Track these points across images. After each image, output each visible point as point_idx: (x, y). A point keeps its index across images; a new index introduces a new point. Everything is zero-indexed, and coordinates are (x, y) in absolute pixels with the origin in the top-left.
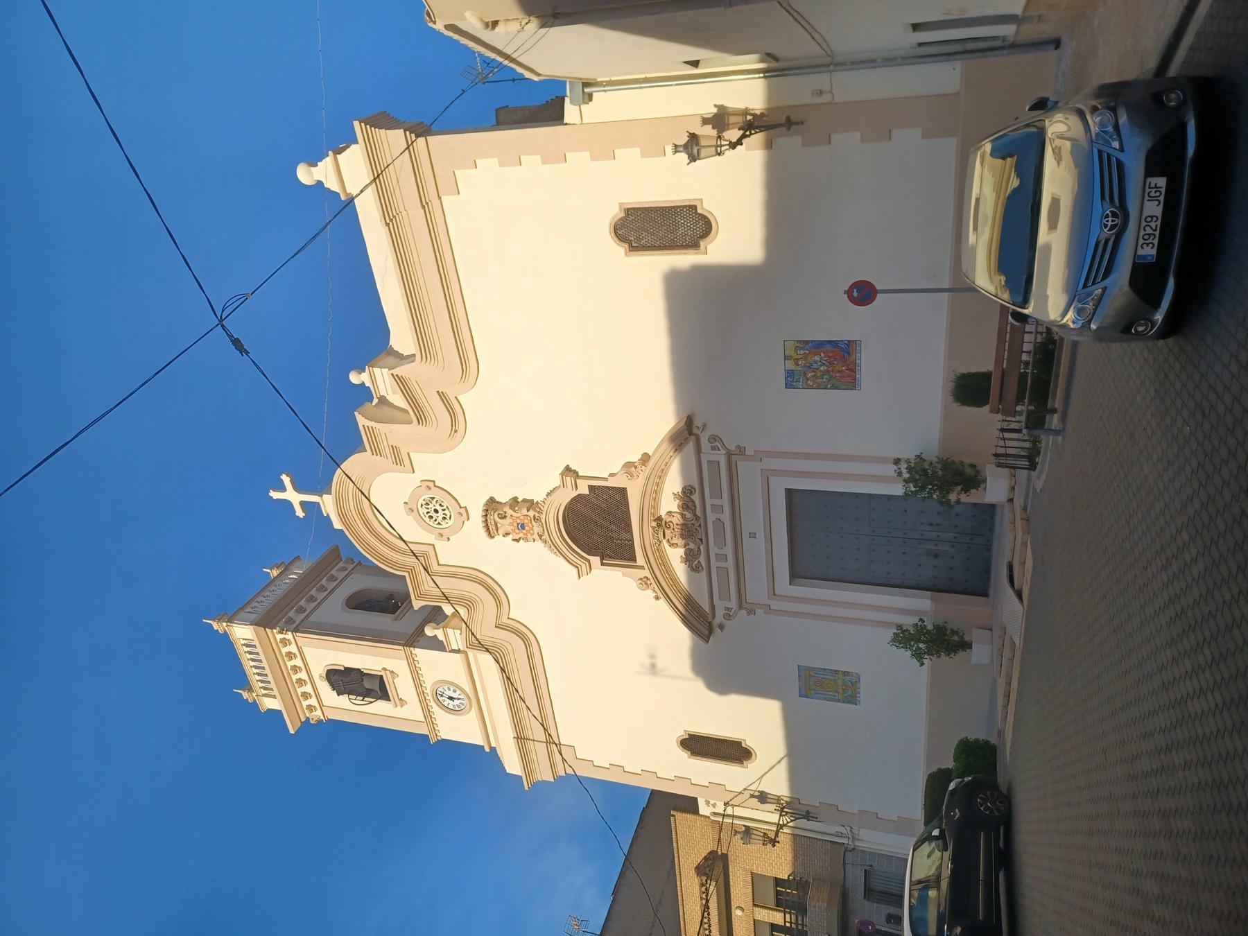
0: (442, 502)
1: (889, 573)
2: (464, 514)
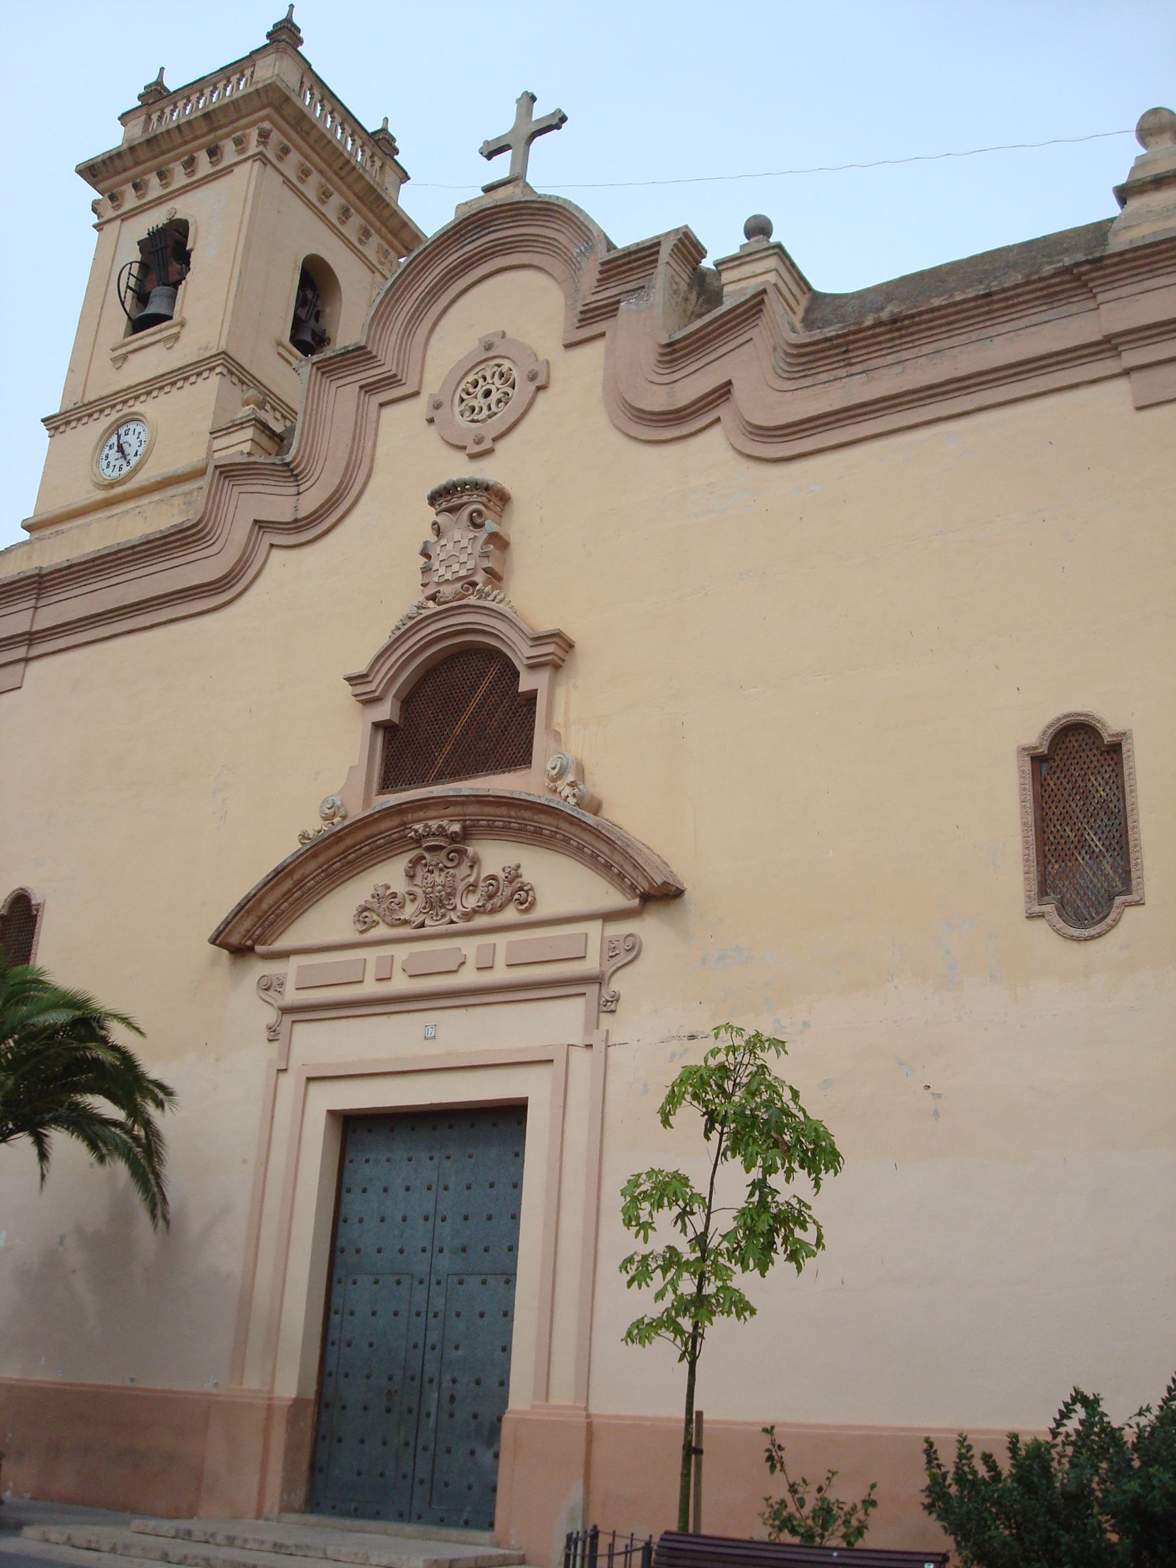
0: (506, 404)
1: (352, 1313)
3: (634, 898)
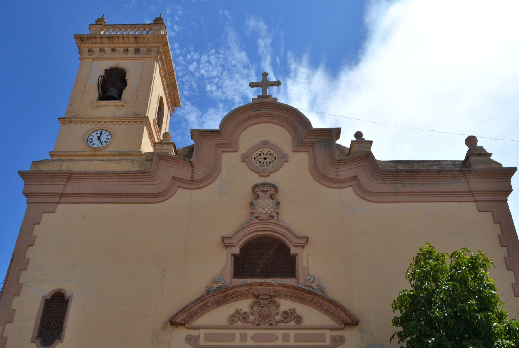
2: (265, 174)
3: (341, 324)
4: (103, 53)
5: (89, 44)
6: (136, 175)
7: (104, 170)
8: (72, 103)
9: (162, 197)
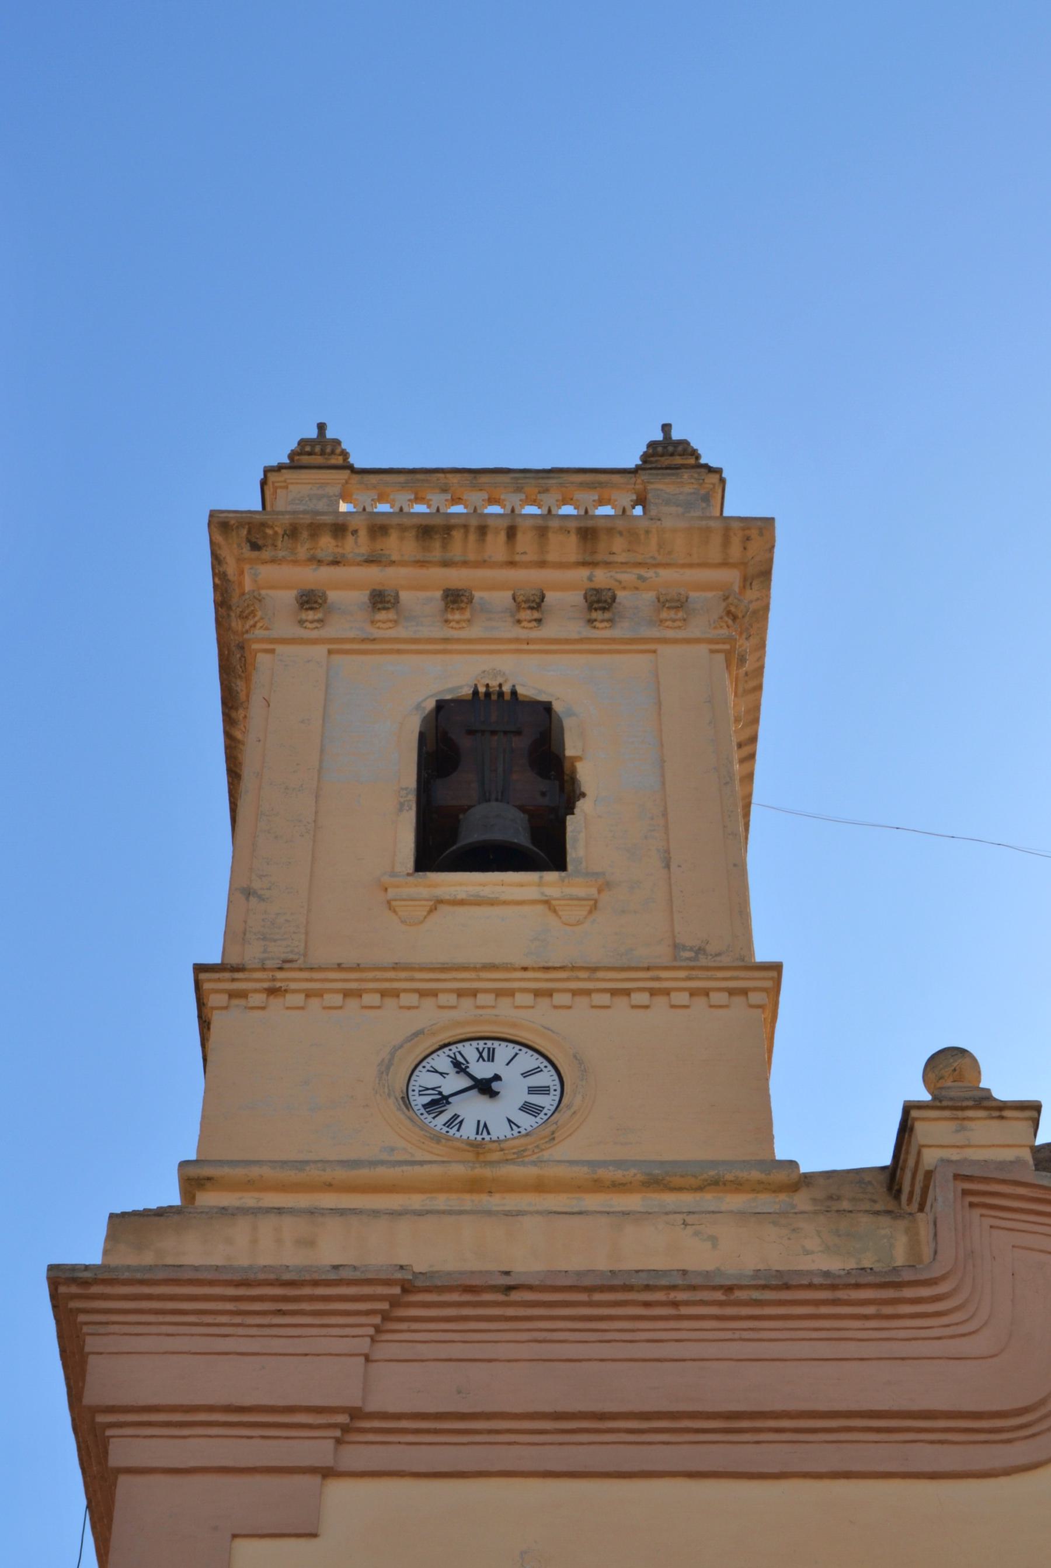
4: (391, 615)
5: (295, 562)
6: (841, 1294)
7: (602, 1264)
8: (256, 885)
9: (1034, 1435)
